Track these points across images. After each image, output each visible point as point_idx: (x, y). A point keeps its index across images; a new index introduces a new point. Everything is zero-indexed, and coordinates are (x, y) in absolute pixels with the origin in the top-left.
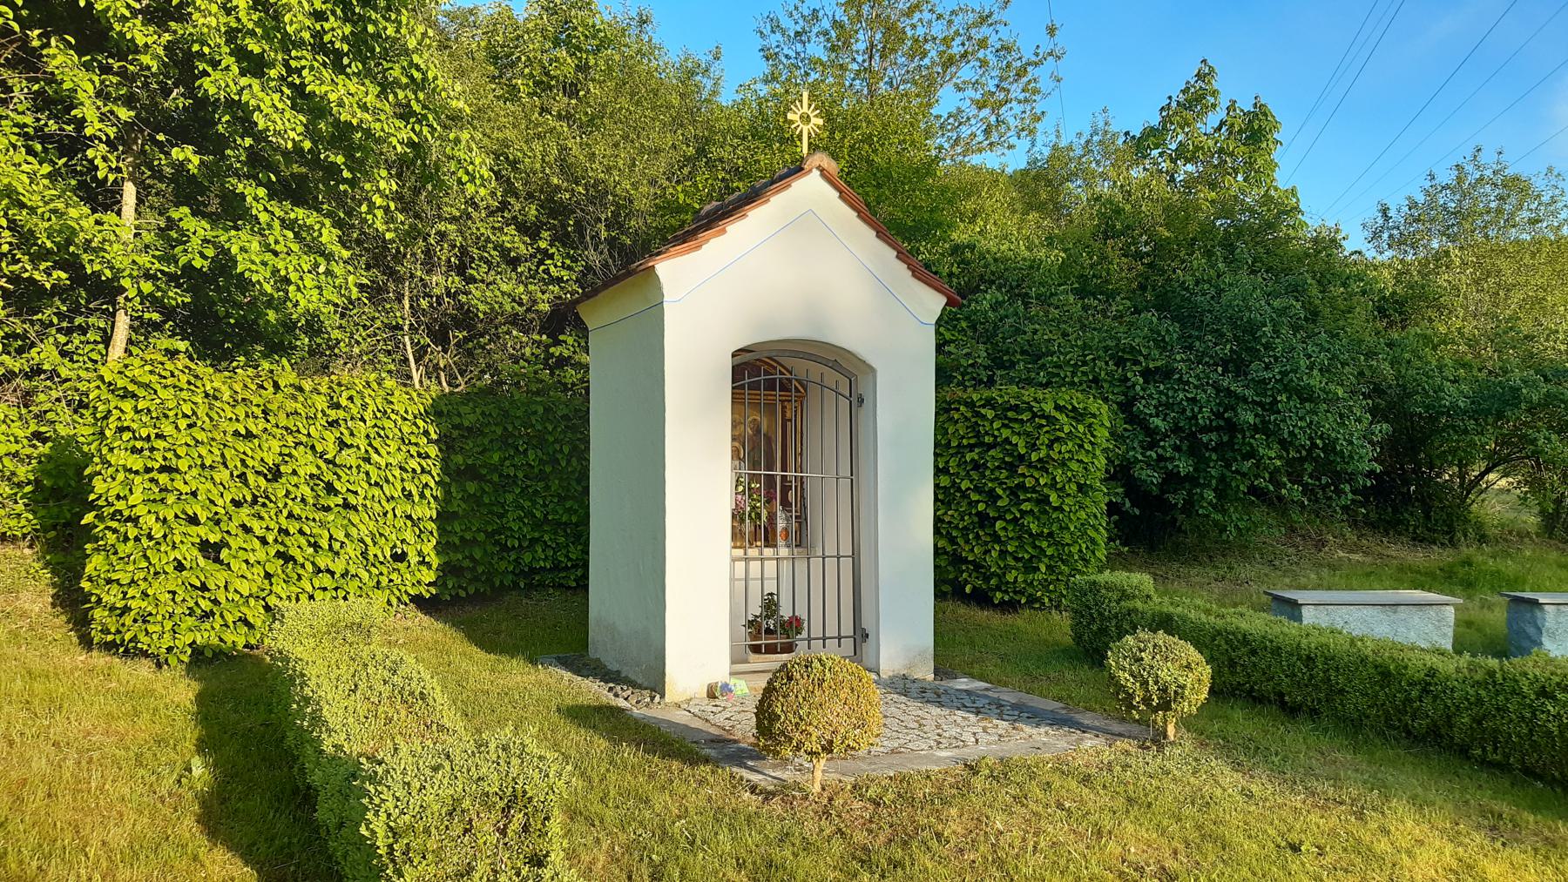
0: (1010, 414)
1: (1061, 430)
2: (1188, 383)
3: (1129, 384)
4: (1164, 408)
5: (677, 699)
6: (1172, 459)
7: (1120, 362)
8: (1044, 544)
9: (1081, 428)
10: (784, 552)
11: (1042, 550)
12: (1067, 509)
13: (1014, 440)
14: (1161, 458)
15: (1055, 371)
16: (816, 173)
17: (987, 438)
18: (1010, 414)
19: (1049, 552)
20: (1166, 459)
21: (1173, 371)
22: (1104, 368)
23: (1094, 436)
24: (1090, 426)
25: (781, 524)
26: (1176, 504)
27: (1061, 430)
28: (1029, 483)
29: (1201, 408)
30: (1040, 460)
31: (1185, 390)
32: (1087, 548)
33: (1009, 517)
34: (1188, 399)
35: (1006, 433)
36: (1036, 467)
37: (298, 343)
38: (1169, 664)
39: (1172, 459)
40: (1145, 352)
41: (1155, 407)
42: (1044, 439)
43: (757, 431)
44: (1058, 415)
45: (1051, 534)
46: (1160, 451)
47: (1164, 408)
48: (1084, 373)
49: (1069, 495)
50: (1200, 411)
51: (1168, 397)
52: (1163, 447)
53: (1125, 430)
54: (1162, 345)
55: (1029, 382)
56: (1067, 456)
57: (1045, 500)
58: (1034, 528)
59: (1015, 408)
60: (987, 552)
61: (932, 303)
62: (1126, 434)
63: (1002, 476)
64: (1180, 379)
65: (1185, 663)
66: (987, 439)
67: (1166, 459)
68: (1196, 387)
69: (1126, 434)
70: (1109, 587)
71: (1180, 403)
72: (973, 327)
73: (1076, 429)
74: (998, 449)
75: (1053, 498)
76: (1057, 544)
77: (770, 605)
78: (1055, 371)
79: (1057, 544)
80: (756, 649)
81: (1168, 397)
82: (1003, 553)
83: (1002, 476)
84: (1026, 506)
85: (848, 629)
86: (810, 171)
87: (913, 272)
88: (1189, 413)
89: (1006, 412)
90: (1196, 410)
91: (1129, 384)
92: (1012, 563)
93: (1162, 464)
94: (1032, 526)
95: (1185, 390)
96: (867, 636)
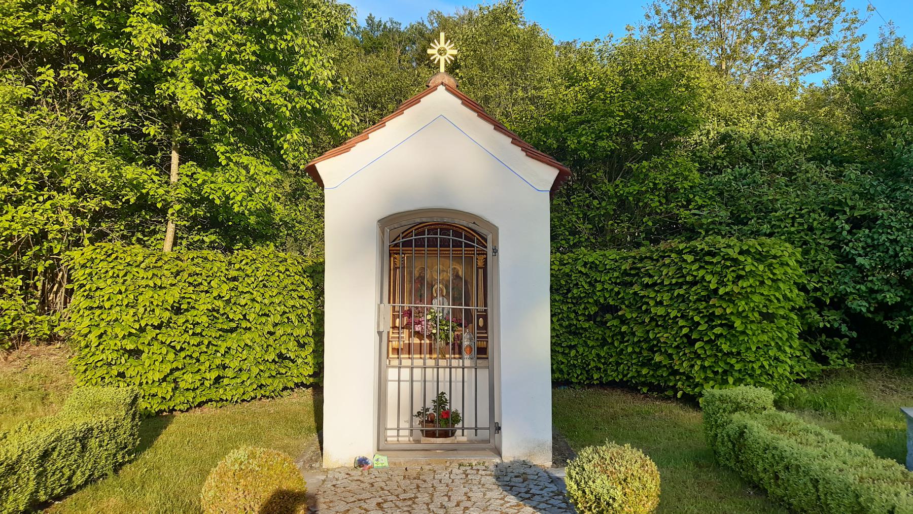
0: (707, 258)
1: (743, 269)
2: (890, 227)
3: (838, 231)
4: (871, 248)
5: (331, 466)
6: (881, 291)
7: (832, 213)
8: (733, 361)
9: (761, 267)
10: (467, 363)
11: (732, 366)
12: (750, 333)
13: (708, 278)
14: (872, 291)
15: (777, 223)
16: (441, 89)
17: (688, 278)
18: (707, 258)
19: (737, 367)
20: (877, 292)
21: (877, 219)
22: (818, 218)
23: (774, 274)
24: (771, 265)
25: (466, 343)
26: (893, 328)
27: (743, 269)
28: (718, 312)
29: (902, 247)
30: (727, 293)
31: (888, 233)
32: (770, 365)
33: (706, 339)
34: (891, 241)
35: (702, 273)
36: (724, 299)
37: (281, 234)
38: (605, 477)
39: (881, 291)
40: (850, 203)
41: (863, 248)
42: (730, 277)
43: (457, 276)
44: (742, 258)
45: (739, 353)
46: (869, 285)
47: (871, 248)
48: (801, 224)
49: (752, 322)
50: (902, 250)
51: (873, 240)
52: (871, 281)
53: (838, 267)
54: (868, 197)
55: (756, 234)
56: (749, 290)
57: (731, 326)
58: (725, 348)
59: (710, 253)
60: (692, 366)
61: (547, 175)
62: (838, 271)
63: (701, 307)
64: (883, 224)
65: (622, 477)
66: (689, 278)
67: (877, 292)
68: (898, 230)
69: (838, 271)
70: (722, 400)
71: (883, 244)
72: (721, 194)
73: (757, 268)
74: (699, 286)
75: (738, 323)
76: (743, 360)
77: (441, 401)
78: (777, 223)
79: (743, 360)
80: (430, 434)
81: (873, 240)
82: (703, 368)
83: (701, 307)
84: (718, 331)
85: (484, 421)
86: (435, 88)
87: (526, 152)
88: (891, 252)
89: (700, 256)
90: (898, 249)
91: (838, 231)
92: (711, 375)
93: (874, 296)
94: (723, 346)
95: (888, 233)
96: (499, 428)
